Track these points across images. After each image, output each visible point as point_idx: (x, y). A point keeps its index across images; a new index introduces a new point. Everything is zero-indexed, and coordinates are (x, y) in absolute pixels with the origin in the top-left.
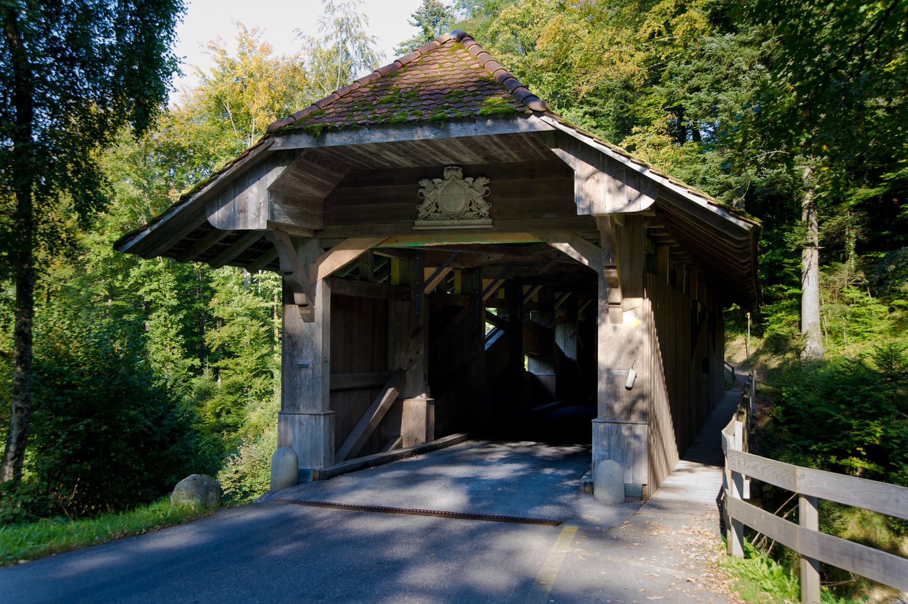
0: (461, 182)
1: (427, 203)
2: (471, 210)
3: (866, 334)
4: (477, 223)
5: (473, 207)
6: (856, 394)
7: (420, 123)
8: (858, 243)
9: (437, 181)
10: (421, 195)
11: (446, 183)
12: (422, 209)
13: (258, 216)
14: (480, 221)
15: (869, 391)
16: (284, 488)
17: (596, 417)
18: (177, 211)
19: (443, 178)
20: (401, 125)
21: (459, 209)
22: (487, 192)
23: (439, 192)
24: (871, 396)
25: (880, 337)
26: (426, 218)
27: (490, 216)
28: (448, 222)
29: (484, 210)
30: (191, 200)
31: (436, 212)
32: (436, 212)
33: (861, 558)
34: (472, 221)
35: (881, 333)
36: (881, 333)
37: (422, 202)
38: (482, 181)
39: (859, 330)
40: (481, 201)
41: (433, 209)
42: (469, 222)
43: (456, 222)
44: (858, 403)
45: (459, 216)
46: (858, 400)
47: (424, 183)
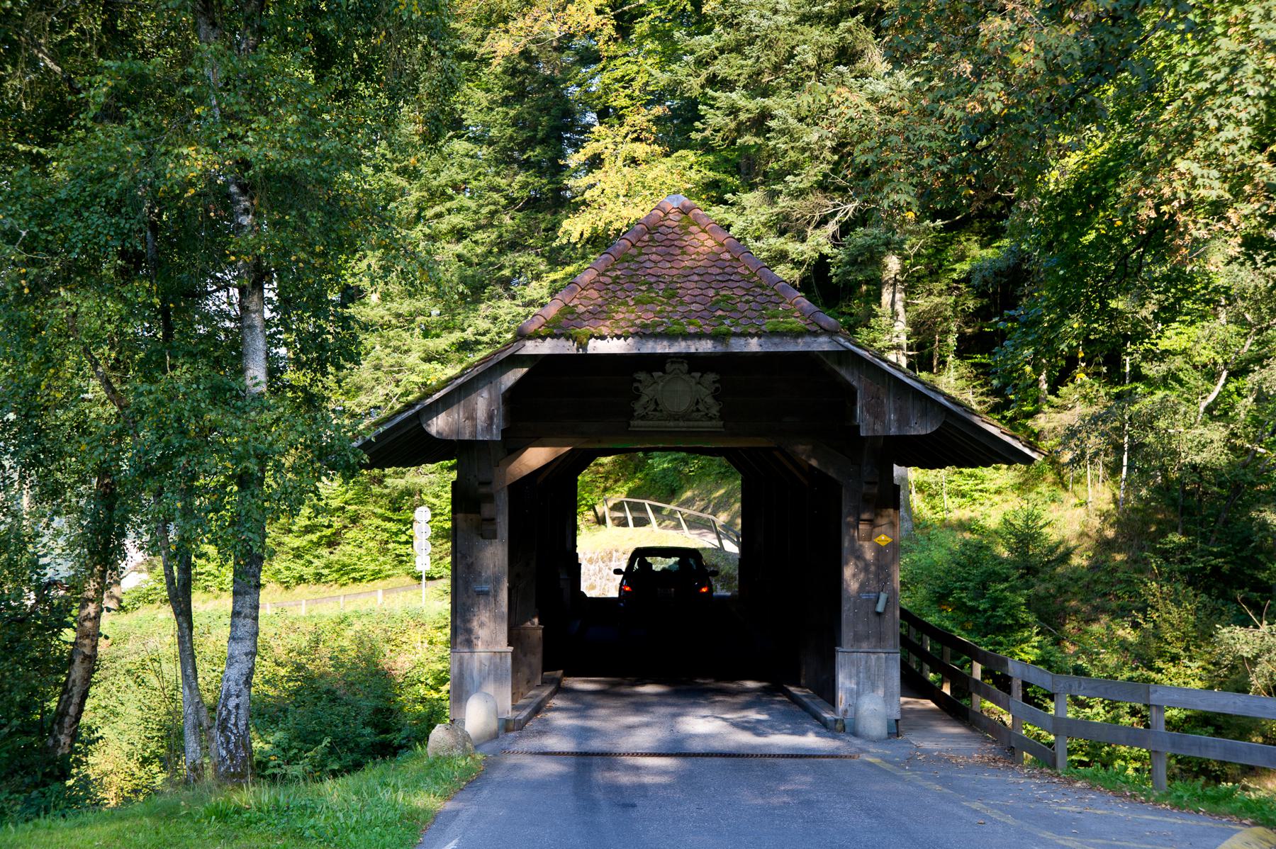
0: (686, 377)
1: (644, 399)
2: (698, 410)
3: (976, 495)
4: (706, 424)
5: (701, 407)
6: (983, 596)
7: (699, 336)
8: (962, 338)
9: (657, 374)
10: (637, 389)
11: (668, 377)
12: (638, 408)
13: (491, 425)
14: (709, 423)
15: (1003, 591)
16: (488, 741)
17: (840, 645)
18: (399, 419)
19: (664, 372)
20: (687, 336)
21: (683, 408)
22: (717, 389)
23: (659, 388)
24: (1006, 598)
25: (996, 498)
26: (643, 418)
27: (721, 418)
28: (672, 424)
29: (714, 411)
30: (418, 407)
31: (655, 410)
32: (655, 410)
33: (1207, 746)
34: (701, 423)
35: (998, 492)
36: (998, 492)
37: (638, 397)
38: (711, 377)
39: (966, 488)
40: (710, 400)
41: (652, 407)
42: (696, 424)
43: (681, 423)
44: (985, 611)
45: (685, 417)
46: (987, 606)
47: (642, 376)
